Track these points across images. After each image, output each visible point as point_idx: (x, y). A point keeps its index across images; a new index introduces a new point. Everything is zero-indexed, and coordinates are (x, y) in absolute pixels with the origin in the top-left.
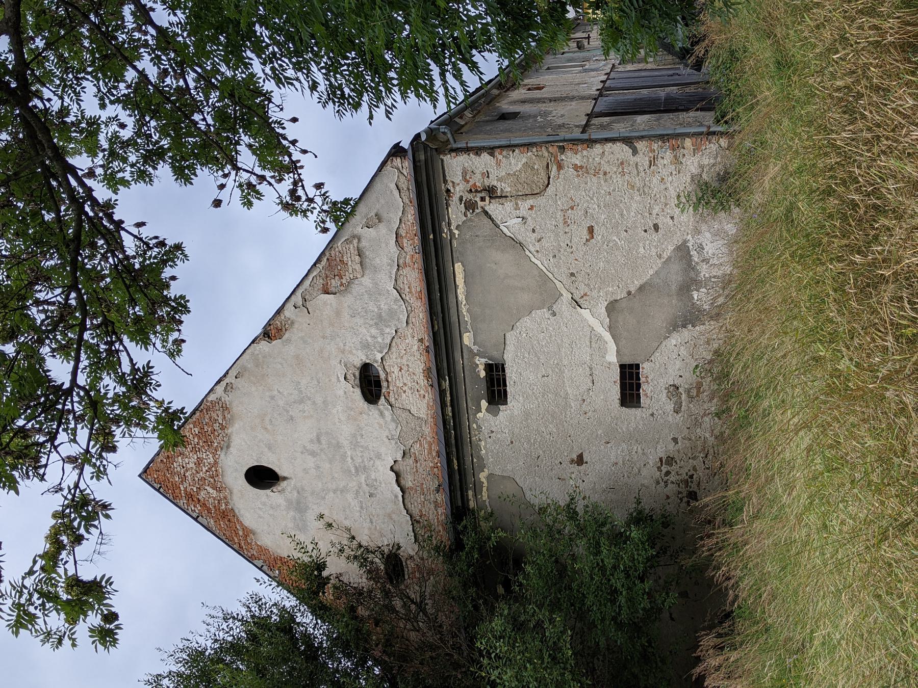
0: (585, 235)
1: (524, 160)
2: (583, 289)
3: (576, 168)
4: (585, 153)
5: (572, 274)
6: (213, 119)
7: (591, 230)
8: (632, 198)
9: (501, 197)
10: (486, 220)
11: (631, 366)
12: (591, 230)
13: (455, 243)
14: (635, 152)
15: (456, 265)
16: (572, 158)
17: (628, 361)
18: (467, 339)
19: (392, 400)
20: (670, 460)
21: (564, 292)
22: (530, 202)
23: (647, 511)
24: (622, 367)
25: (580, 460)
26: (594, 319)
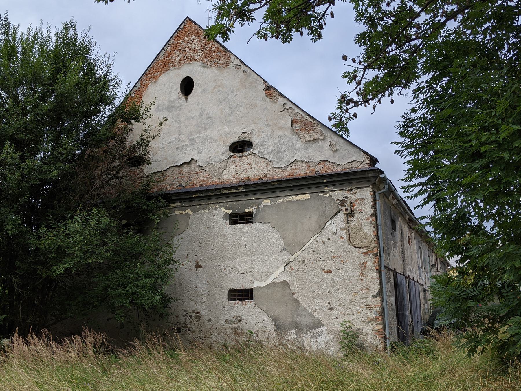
0: (327, 269)
2: (296, 268)
3: (365, 263)
5: (304, 261)
7: (329, 272)
8: (348, 295)
10: (334, 212)
11: (252, 295)
12: (329, 272)
14: (374, 297)
15: (309, 195)
16: (371, 260)
17: (255, 293)
18: (267, 202)
19: (232, 159)
20: (198, 318)
24: (251, 290)
25: (198, 266)
26: (278, 274)
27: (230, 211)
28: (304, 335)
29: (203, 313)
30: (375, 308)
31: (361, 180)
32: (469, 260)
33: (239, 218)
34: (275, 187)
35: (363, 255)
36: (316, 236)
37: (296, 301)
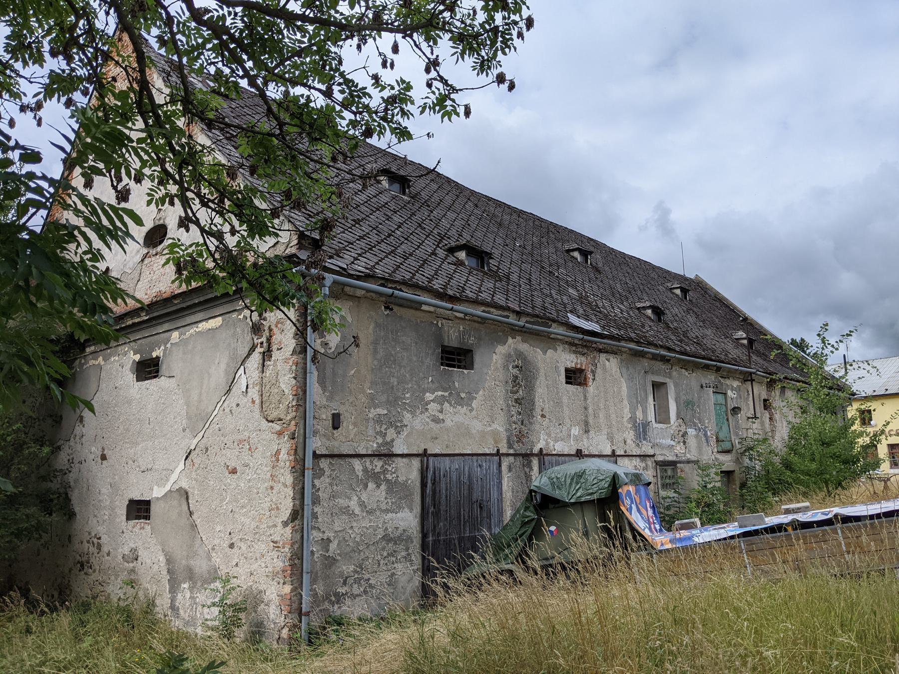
0: (232, 464)
1: (286, 391)
2: (197, 461)
3: (278, 452)
4: (288, 463)
5: (207, 449)
6: (296, 98)
7: (234, 471)
8: (253, 519)
9: (264, 366)
10: (247, 350)
11: (148, 510)
12: (234, 471)
13: (234, 315)
14: (285, 524)
15: (220, 318)
16: (285, 445)
17: (153, 508)
18: (175, 335)
19: (147, 261)
20: (99, 547)
21: (195, 441)
22: (258, 401)
23: (498, 639)
24: (148, 503)
25: (104, 457)
26: (179, 476)
27: (137, 358)
28: (198, 595)
29: (105, 539)
30: (284, 548)
31: (197, 309)
32: (119, 104)
33: (148, 369)
34: (179, 307)
35: (276, 436)
36: (224, 398)
37: (194, 526)
